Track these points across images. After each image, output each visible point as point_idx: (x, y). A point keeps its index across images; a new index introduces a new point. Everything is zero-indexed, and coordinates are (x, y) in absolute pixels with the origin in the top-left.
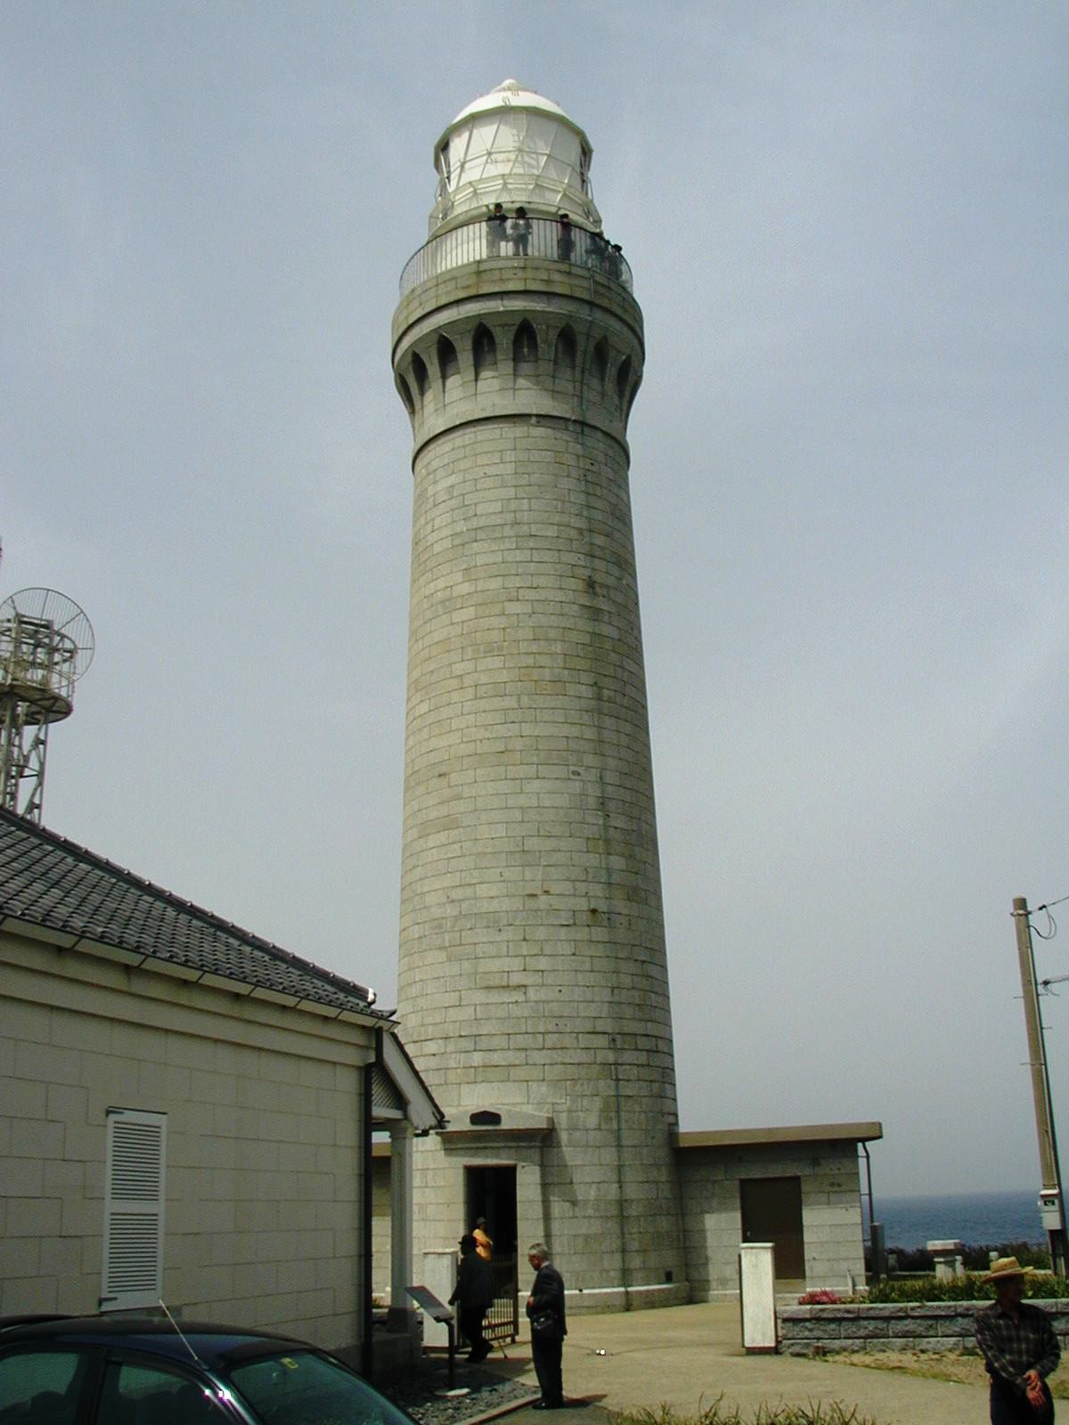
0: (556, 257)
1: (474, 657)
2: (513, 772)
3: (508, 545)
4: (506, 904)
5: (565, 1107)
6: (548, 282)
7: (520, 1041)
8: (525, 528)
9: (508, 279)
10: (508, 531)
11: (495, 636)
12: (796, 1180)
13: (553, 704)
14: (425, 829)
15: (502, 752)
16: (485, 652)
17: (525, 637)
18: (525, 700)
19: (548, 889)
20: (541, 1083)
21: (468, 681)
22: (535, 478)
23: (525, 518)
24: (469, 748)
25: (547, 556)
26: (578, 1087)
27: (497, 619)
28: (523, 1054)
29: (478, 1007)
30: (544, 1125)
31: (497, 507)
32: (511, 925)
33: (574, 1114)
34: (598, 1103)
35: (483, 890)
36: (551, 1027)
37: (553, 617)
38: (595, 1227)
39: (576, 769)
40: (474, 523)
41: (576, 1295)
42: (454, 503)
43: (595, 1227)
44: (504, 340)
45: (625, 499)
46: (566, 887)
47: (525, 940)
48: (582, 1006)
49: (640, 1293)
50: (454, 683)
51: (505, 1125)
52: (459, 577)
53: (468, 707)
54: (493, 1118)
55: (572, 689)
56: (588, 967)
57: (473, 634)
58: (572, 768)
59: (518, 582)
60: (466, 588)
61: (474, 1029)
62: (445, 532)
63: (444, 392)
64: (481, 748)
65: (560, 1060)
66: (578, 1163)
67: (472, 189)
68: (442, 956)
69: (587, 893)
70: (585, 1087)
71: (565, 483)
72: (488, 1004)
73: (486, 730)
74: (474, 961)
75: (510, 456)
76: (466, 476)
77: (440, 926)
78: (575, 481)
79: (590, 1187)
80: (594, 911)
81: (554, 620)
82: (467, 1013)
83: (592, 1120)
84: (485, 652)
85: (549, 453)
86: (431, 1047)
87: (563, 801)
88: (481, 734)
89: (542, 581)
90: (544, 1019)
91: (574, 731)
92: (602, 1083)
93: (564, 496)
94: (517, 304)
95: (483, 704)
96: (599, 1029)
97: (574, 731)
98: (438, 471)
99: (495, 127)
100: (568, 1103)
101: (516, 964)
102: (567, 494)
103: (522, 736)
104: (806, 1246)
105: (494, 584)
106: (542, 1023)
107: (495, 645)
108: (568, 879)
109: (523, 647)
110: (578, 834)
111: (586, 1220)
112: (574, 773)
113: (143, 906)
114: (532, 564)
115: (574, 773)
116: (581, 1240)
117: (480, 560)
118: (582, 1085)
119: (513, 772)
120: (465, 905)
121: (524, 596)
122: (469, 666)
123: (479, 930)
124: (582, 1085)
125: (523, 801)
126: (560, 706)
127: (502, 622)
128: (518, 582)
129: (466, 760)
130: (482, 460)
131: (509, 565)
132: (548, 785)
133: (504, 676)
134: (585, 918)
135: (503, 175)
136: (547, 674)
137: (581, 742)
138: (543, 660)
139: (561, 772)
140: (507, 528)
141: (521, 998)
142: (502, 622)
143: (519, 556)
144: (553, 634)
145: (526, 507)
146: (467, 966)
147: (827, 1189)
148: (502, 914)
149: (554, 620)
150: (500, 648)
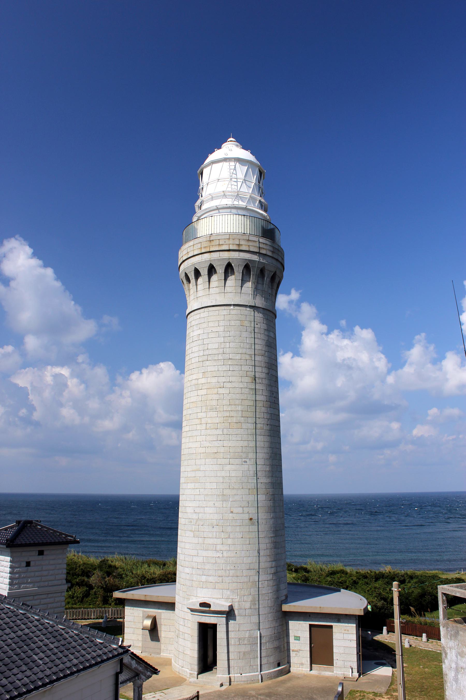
0: (234, 276)
1: (206, 411)
2: (220, 461)
3: (220, 363)
4: (216, 516)
5: (237, 600)
6: (239, 245)
7: (220, 573)
8: (228, 356)
9: (222, 244)
10: (220, 357)
11: (214, 403)
12: (331, 627)
13: (236, 433)
14: (226, 198)
15: (216, 453)
16: (210, 410)
17: (226, 404)
18: (225, 431)
19: (232, 511)
20: (228, 590)
21: (203, 421)
22: (232, 333)
23: (228, 351)
24: (203, 450)
25: (236, 368)
26: (242, 592)
27: (216, 396)
28: (221, 578)
29: (204, 557)
30: (227, 609)
31: (216, 346)
32: (218, 525)
33: (240, 603)
34: (250, 598)
35: (207, 510)
36: (232, 568)
37: (237, 395)
38: (248, 648)
39: (245, 460)
40: (207, 352)
41: (239, 676)
42: (200, 342)
43: (248, 648)
44: (220, 270)
45: (283, 253)
46: (240, 510)
47: (223, 532)
48: (245, 559)
49: (266, 673)
50: (198, 421)
51: (212, 608)
52: (201, 375)
53: (203, 432)
54: (208, 605)
55: (244, 426)
56: (248, 542)
57: (206, 401)
58: (244, 460)
59: (223, 379)
60: (203, 381)
61: (203, 566)
62: (196, 355)
63: (197, 285)
64: (208, 450)
65: (235, 581)
66: (241, 623)
67: (211, 196)
68: (192, 534)
69: (248, 512)
70: (246, 591)
71: (245, 334)
72: (208, 557)
73: (210, 443)
74: (203, 538)
75: (222, 323)
76: (205, 331)
77: (191, 522)
78: (249, 333)
79: (246, 632)
80: (251, 519)
81: (238, 396)
82: (200, 560)
83: (248, 605)
84: (210, 410)
85: (238, 321)
86: (187, 570)
87: (240, 474)
88: (208, 444)
89: (232, 379)
90: (230, 564)
91: (245, 444)
92: (252, 590)
93: (244, 340)
94: (226, 255)
95: (209, 432)
96: (251, 568)
97: (245, 444)
98: (194, 326)
99: (223, 163)
100: (238, 599)
101: (219, 541)
102: (245, 340)
103: (223, 447)
104: (334, 654)
105: (214, 380)
106: (228, 566)
107: (214, 406)
108: (241, 507)
109: (225, 408)
110: (245, 487)
111: (244, 646)
112: (244, 462)
113: (75, 616)
114: (230, 372)
115: (244, 462)
116: (242, 654)
117: (210, 369)
118: (244, 591)
119: (220, 461)
120: (200, 515)
121: (226, 386)
122: (203, 415)
123: (206, 526)
124: (244, 591)
125: (223, 474)
126: (239, 433)
127: (216, 397)
128: (223, 379)
129: (202, 455)
130: (211, 324)
131: (220, 372)
132: (233, 467)
133: (217, 420)
134: (248, 521)
135: (223, 191)
136: (234, 420)
137: (248, 448)
138: (232, 414)
139: (238, 461)
140: (220, 356)
141: (221, 556)
142: (216, 397)
143: (225, 368)
144: (237, 402)
145: (228, 346)
146: (201, 540)
147: (343, 632)
148: (214, 520)
149: (238, 396)
150: (216, 408)
